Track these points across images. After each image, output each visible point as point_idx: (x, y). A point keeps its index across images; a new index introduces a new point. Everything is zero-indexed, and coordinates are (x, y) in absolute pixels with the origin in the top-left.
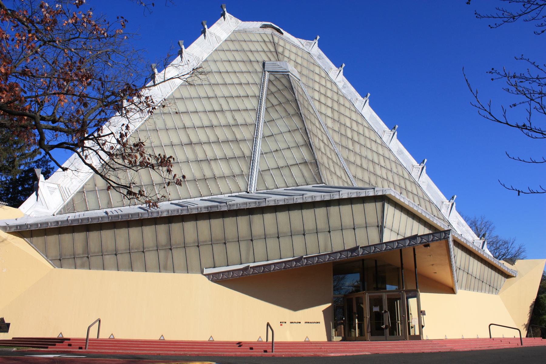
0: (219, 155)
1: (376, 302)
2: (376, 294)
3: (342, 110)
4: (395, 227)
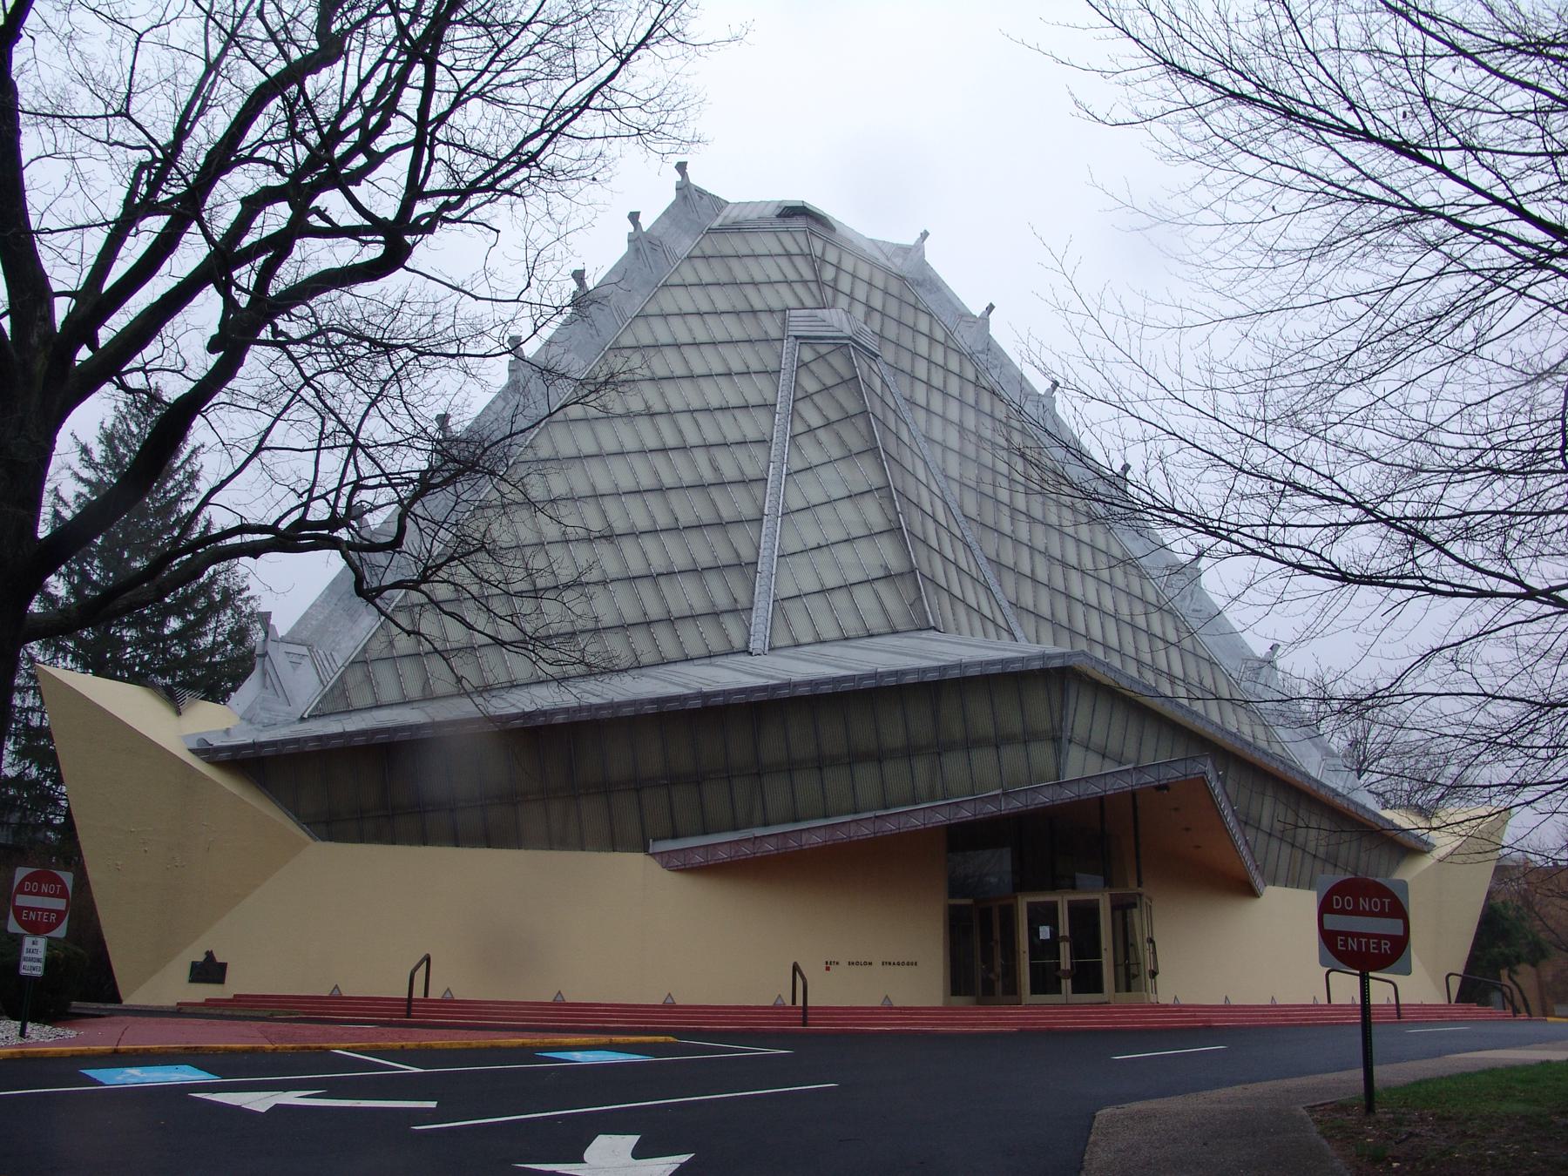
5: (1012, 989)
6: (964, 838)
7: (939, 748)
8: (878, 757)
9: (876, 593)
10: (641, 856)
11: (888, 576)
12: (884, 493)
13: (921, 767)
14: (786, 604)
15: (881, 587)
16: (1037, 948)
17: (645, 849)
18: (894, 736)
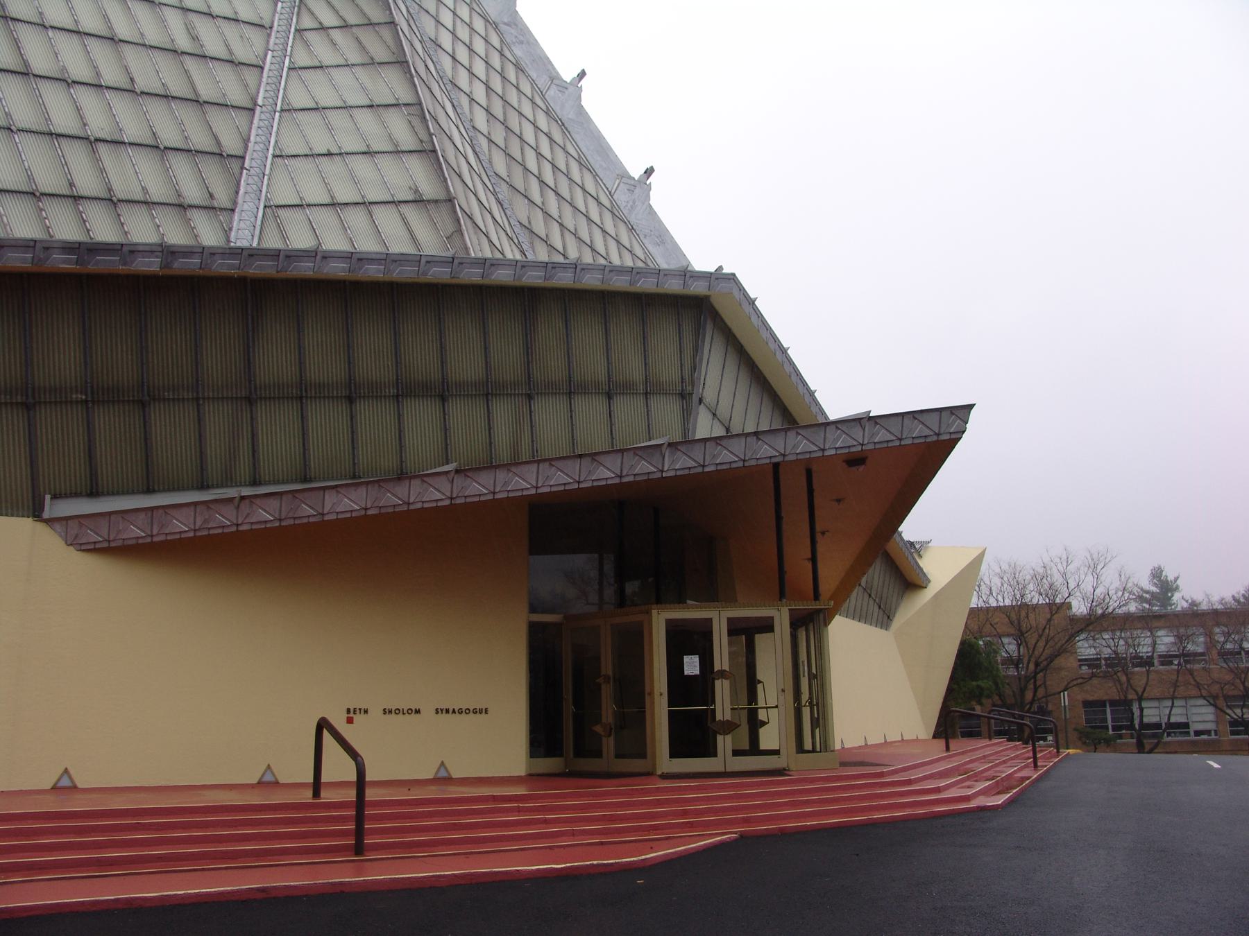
0: (133, 130)
1: (688, 638)
2: (691, 613)
3: (513, 97)
4: (723, 410)
5: (638, 747)
6: (554, 523)
7: (530, 390)
8: (442, 392)
9: (404, 219)
10: (26, 524)
11: (419, 201)
12: (413, 110)
13: (503, 411)
14: (281, 212)
15: (410, 212)
16: (681, 687)
17: (36, 512)
18: (465, 364)
